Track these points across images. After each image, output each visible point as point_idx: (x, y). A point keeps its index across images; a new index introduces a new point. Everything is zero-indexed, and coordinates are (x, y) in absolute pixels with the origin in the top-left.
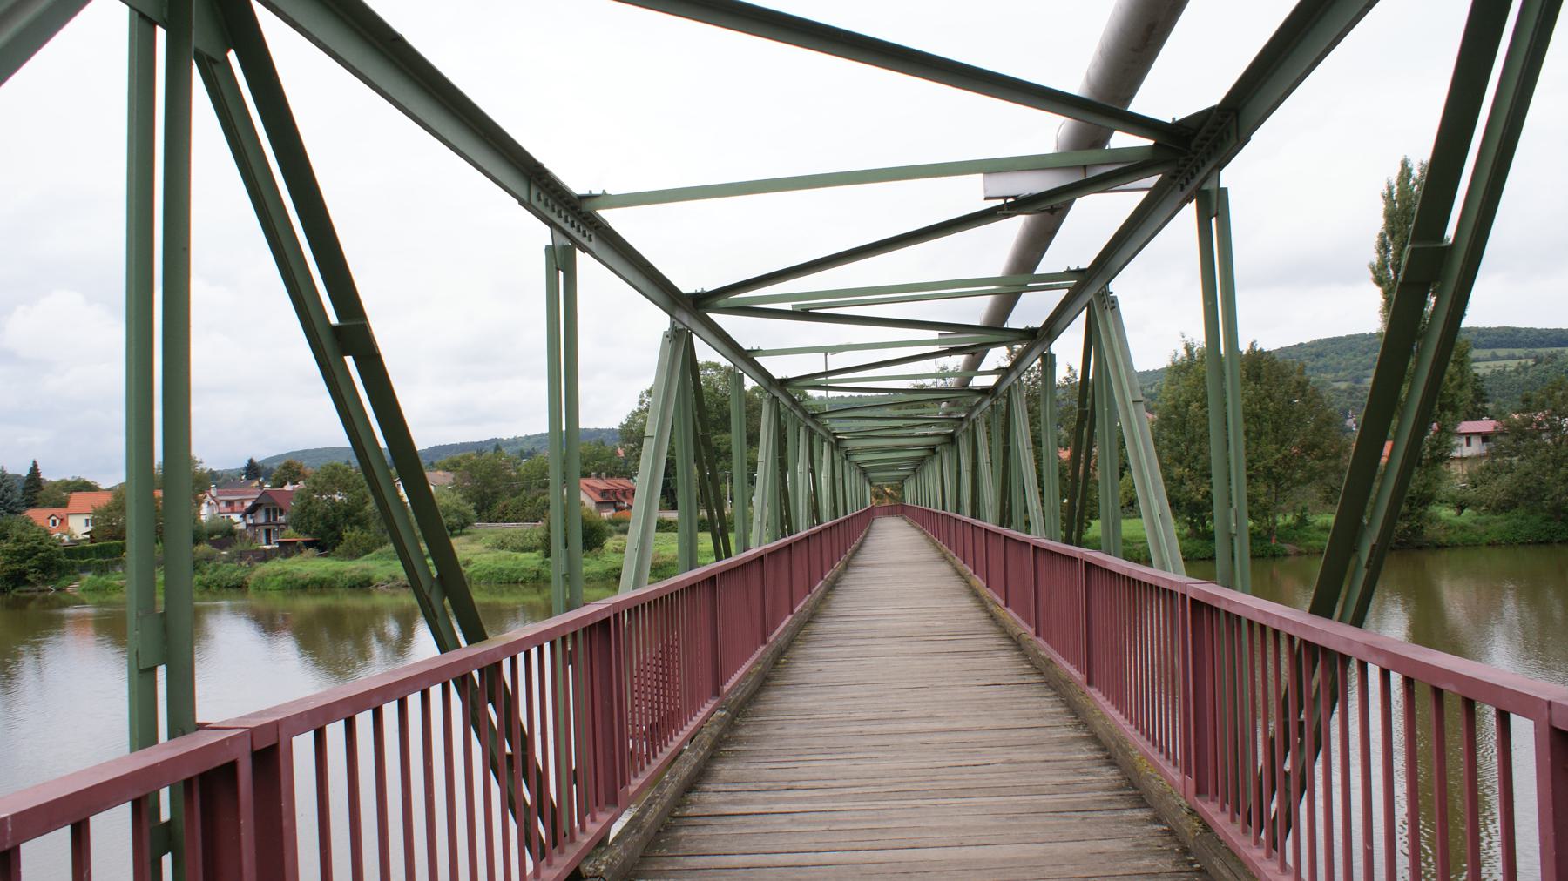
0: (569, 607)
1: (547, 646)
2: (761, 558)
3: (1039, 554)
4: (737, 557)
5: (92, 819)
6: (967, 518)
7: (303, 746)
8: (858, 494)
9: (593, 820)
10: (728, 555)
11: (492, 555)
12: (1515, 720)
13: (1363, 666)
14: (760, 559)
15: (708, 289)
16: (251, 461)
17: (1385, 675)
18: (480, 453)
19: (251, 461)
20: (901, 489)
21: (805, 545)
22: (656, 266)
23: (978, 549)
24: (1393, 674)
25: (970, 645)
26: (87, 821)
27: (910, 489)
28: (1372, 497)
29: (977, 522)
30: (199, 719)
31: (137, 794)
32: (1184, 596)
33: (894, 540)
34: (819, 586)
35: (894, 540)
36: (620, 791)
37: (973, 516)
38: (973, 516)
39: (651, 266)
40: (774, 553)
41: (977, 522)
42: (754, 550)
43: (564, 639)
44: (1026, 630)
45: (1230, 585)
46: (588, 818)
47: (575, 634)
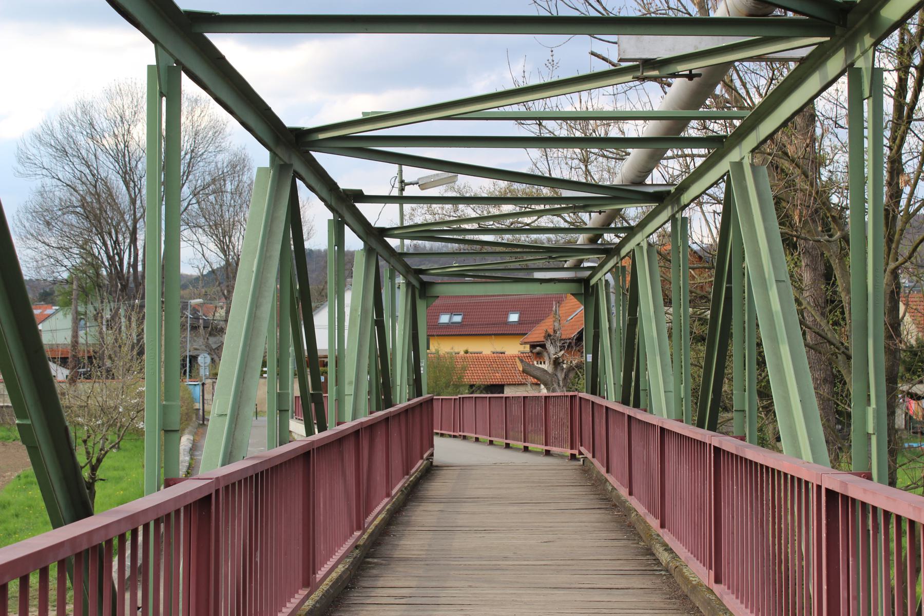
1: (53, 573)
2: (421, 404)
3: (671, 448)
4: (332, 430)
6: (611, 400)
10: (322, 428)
14: (356, 433)
21: (403, 418)
22: (227, 58)
28: (163, 369)
31: (60, 558)
32: (710, 445)
36: (312, 577)
40: (371, 428)
42: (349, 424)
43: (157, 522)
47: (178, 512)
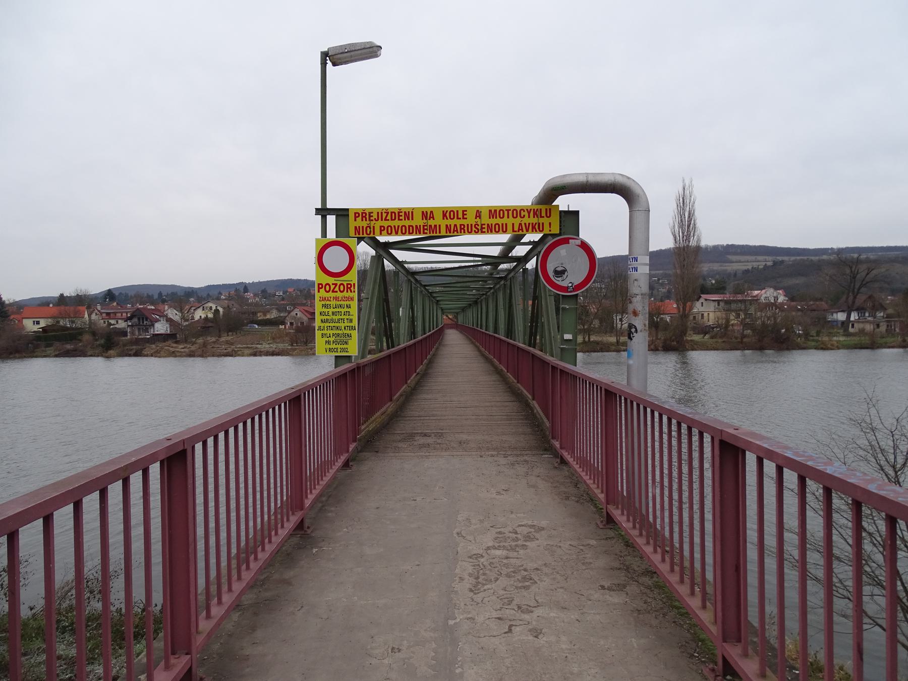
5: (109, 487)
7: (199, 447)
8: (445, 319)
10: (393, 347)
12: (766, 462)
13: (620, 397)
16: (62, 295)
18: (236, 290)
19: (62, 295)
20: (456, 317)
23: (494, 349)
24: (705, 434)
26: (107, 488)
27: (460, 318)
30: (626, 252)
31: (9, 532)
33: (453, 337)
34: (413, 379)
35: (453, 337)
45: (534, 347)
46: (244, 567)
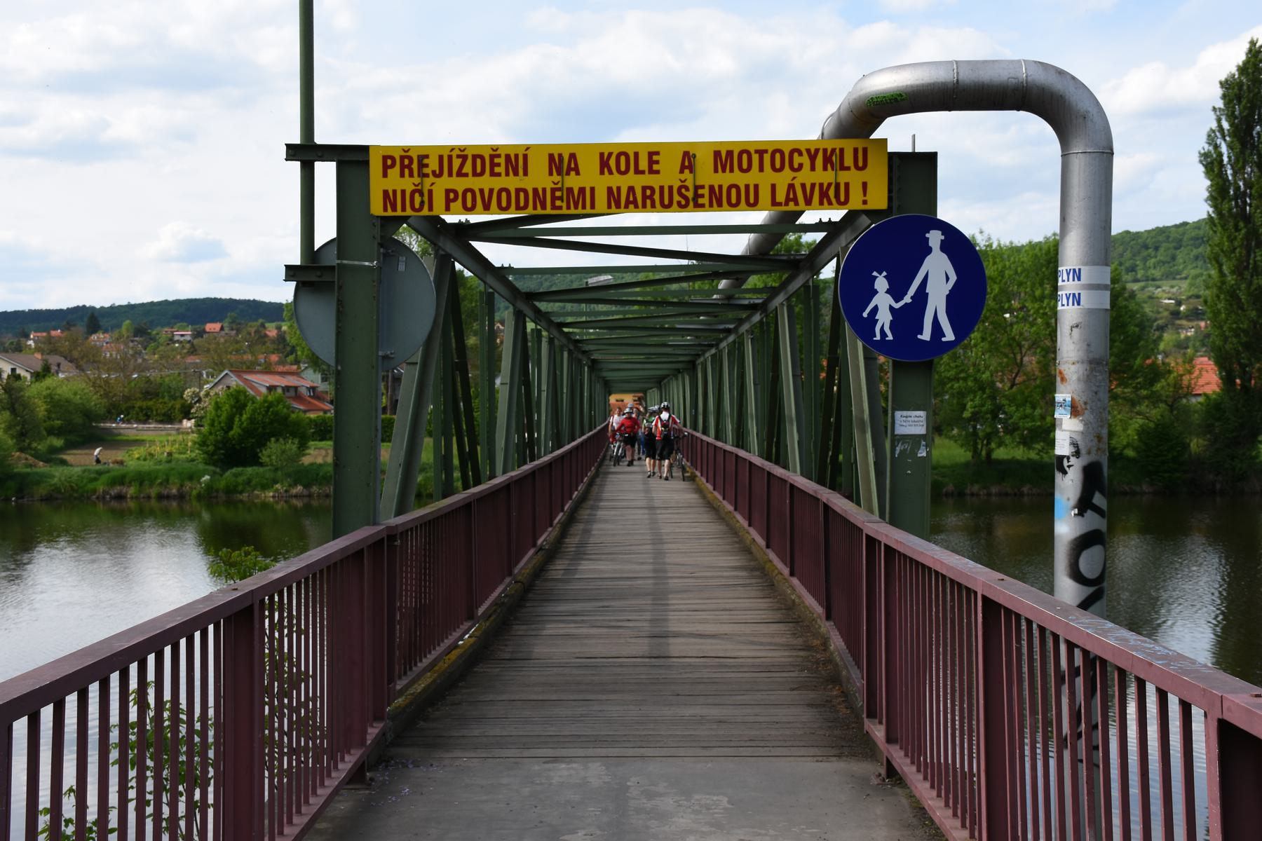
0: (445, 496)
9: (343, 760)
11: (145, 436)
13: (1141, 685)
15: (515, 266)
17: (1186, 708)
24: (1170, 696)
25: (778, 640)
29: (719, 444)
37: (717, 438)
38: (717, 438)
39: (486, 260)
41: (719, 444)
44: (813, 605)
47: (328, 567)
